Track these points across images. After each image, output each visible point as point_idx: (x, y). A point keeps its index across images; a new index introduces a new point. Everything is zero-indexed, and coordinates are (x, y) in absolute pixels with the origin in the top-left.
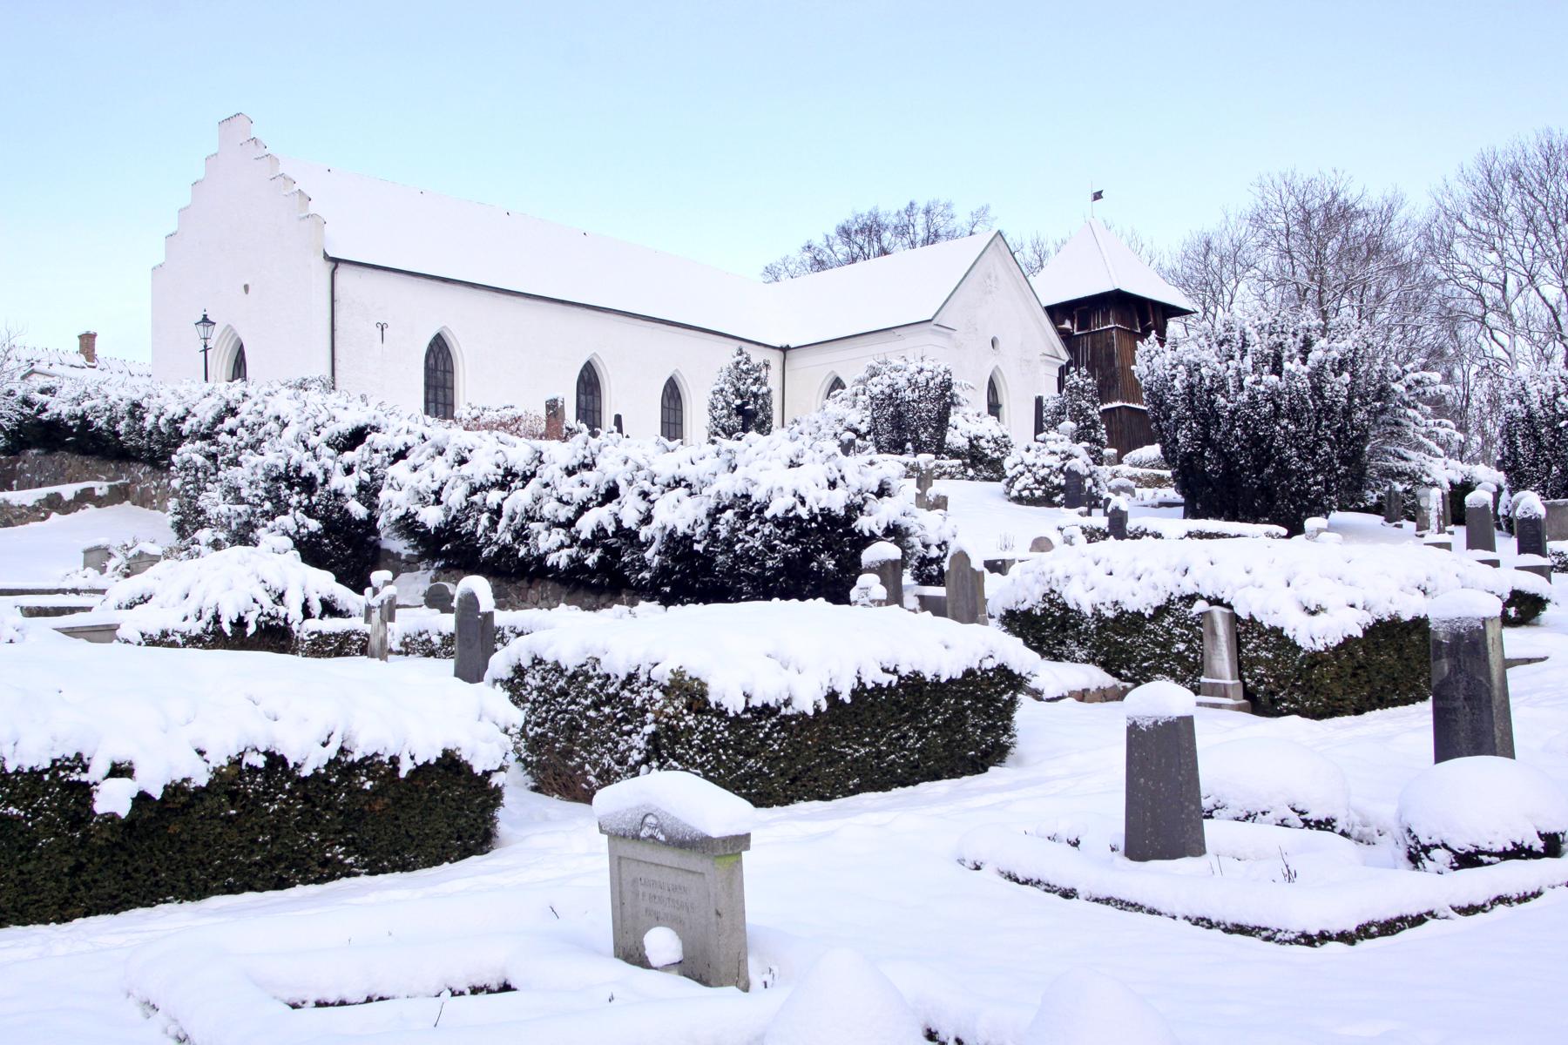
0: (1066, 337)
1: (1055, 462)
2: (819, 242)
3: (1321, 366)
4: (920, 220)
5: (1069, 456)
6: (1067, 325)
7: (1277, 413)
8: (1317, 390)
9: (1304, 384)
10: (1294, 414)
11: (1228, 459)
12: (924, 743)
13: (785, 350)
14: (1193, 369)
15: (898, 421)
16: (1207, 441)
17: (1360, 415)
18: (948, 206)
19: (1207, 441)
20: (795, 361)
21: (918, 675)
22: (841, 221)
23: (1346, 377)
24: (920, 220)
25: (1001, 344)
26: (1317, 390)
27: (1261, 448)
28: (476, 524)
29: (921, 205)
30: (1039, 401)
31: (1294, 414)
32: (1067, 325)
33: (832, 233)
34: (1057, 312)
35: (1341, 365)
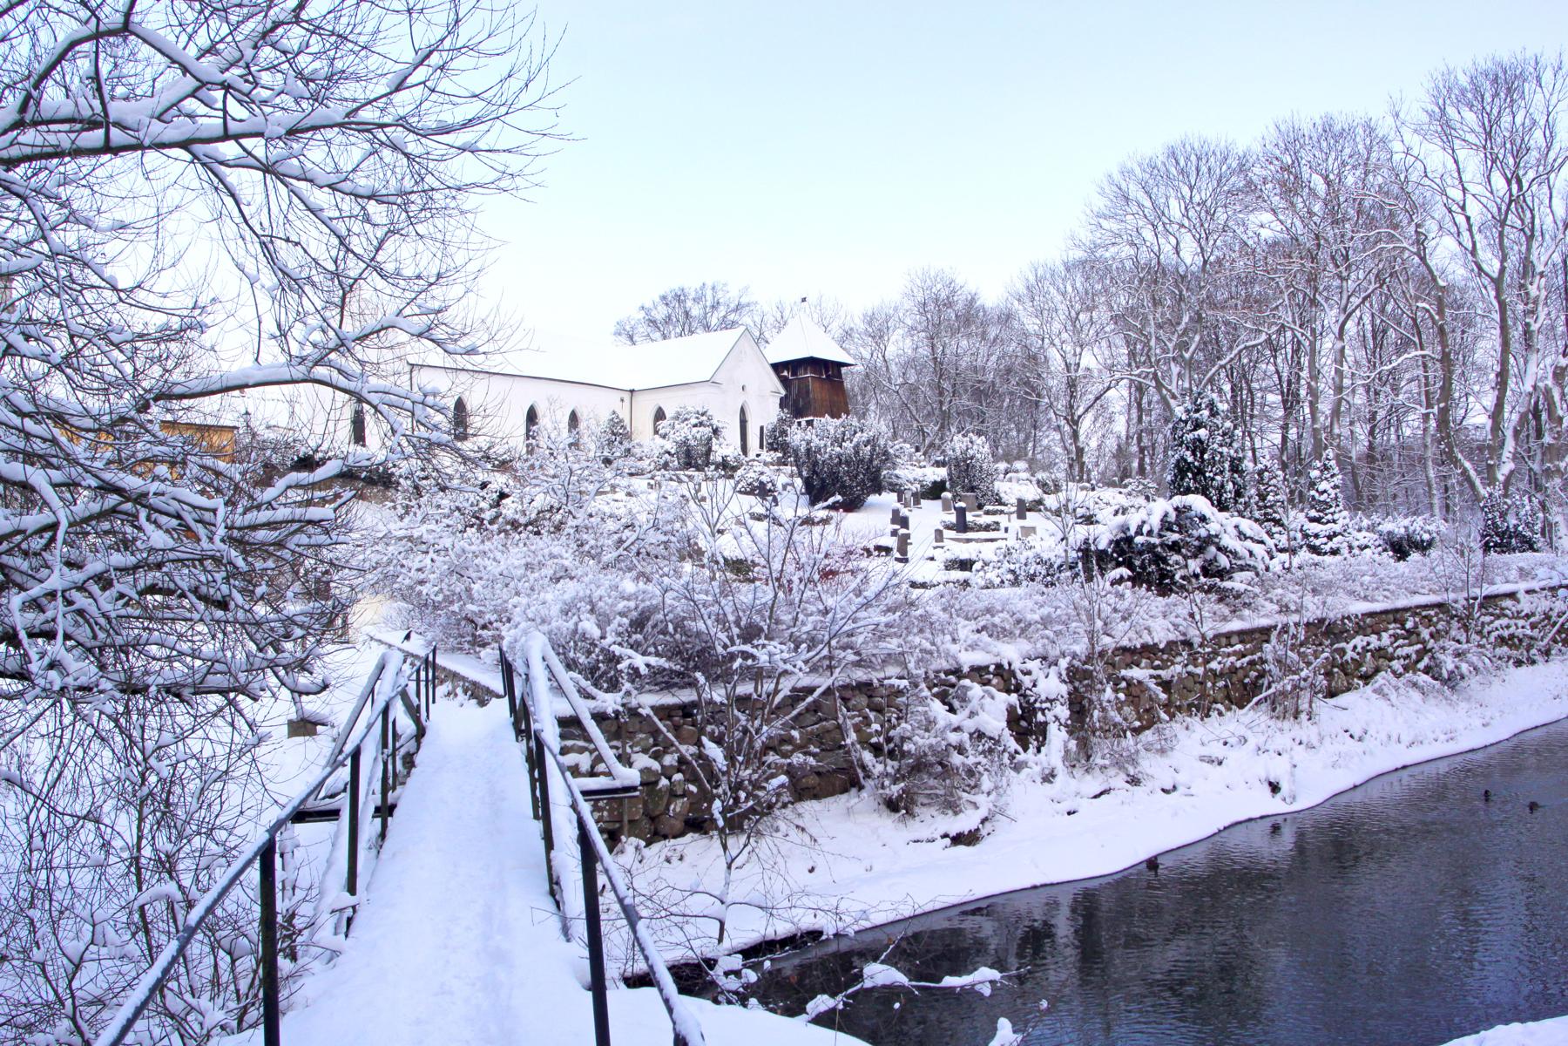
0: (784, 381)
1: (755, 476)
2: (648, 305)
3: (858, 443)
4: (709, 294)
5: (762, 473)
6: (785, 373)
7: (840, 463)
8: (857, 453)
9: (850, 451)
10: (848, 463)
11: (823, 480)
12: (1462, 452)
13: (632, 391)
14: (808, 443)
15: (688, 453)
16: (815, 472)
17: (875, 462)
18: (725, 285)
19: (815, 472)
20: (637, 398)
21: (949, 304)
22: (662, 293)
23: (869, 448)
24: (709, 294)
25: (747, 389)
26: (857, 453)
27: (834, 476)
28: (1139, 927)
29: (709, 285)
30: (762, 428)
31: (848, 463)
32: (785, 373)
33: (657, 299)
34: (777, 367)
35: (867, 443)
